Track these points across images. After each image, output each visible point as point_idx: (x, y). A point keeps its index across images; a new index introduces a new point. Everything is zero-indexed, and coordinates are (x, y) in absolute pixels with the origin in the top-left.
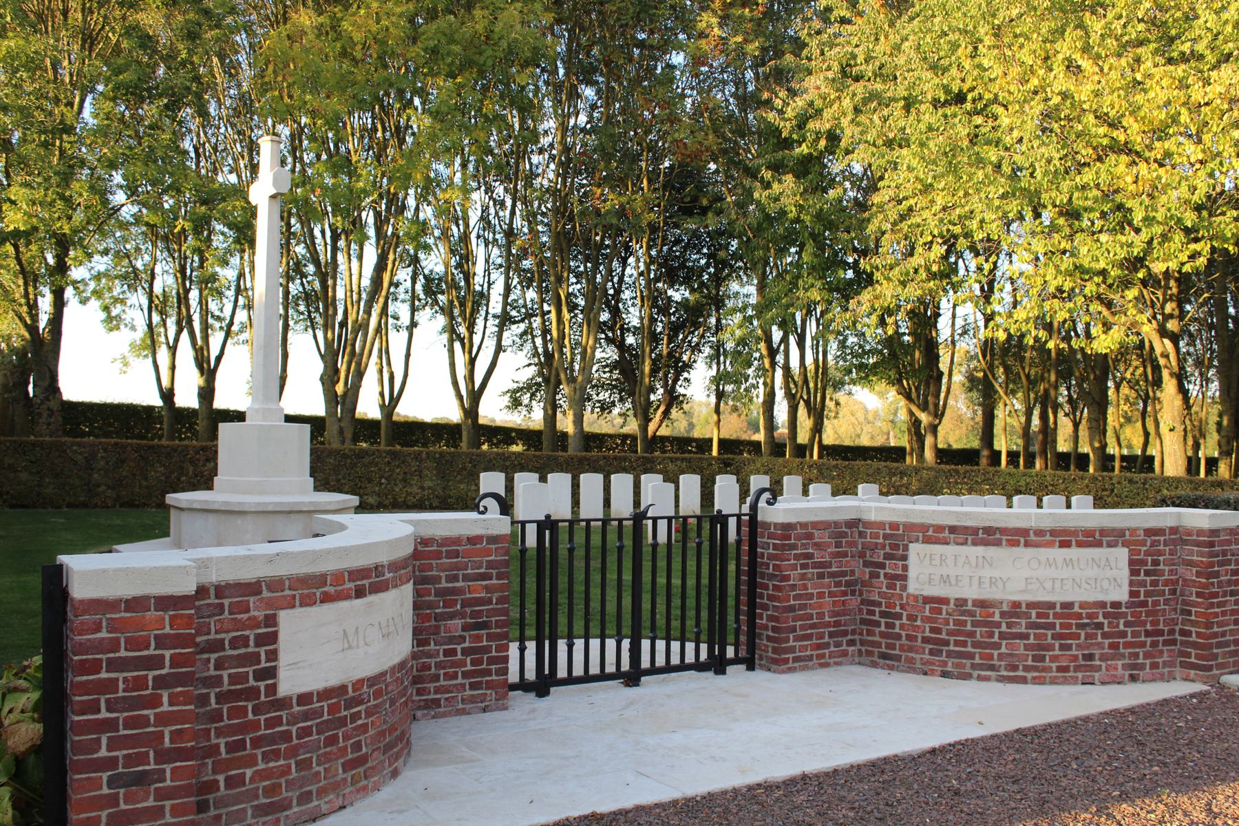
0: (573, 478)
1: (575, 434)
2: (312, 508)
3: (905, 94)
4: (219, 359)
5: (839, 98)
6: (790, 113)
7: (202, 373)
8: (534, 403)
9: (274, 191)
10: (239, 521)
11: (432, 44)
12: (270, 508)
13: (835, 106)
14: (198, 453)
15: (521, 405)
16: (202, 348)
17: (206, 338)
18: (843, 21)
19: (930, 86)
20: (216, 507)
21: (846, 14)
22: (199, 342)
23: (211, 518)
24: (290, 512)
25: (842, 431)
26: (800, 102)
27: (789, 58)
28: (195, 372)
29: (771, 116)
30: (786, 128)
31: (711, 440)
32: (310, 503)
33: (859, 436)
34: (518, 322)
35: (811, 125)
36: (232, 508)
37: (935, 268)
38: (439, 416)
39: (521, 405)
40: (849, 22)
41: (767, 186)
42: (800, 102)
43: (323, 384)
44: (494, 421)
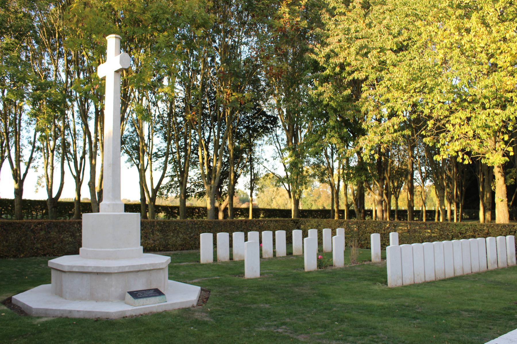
0: (245, 234)
1: (211, 209)
2: (152, 268)
3: (381, 45)
4: (25, 175)
5: (349, 47)
6: (323, 54)
7: (16, 181)
8: (169, 193)
9: (119, 67)
10: (106, 279)
11: (155, 13)
12: (127, 270)
13: (346, 52)
14: (36, 226)
15: (163, 194)
16: (16, 170)
17: (18, 165)
18: (341, 14)
19: (390, 44)
20: (90, 270)
21: (343, 10)
22: (15, 167)
23: (86, 277)
24: (138, 271)
25: (279, 202)
26: (327, 50)
27: (318, 30)
28: (13, 181)
29: (313, 56)
30: (322, 61)
31: (290, 210)
32: (151, 264)
33: (286, 204)
34: (161, 157)
35: (331, 60)
36: (102, 271)
37: (396, 127)
38: (67, 197)
39: (163, 194)
40: (344, 14)
41: (316, 88)
42: (327, 50)
43: (90, 187)
44: (129, 201)
